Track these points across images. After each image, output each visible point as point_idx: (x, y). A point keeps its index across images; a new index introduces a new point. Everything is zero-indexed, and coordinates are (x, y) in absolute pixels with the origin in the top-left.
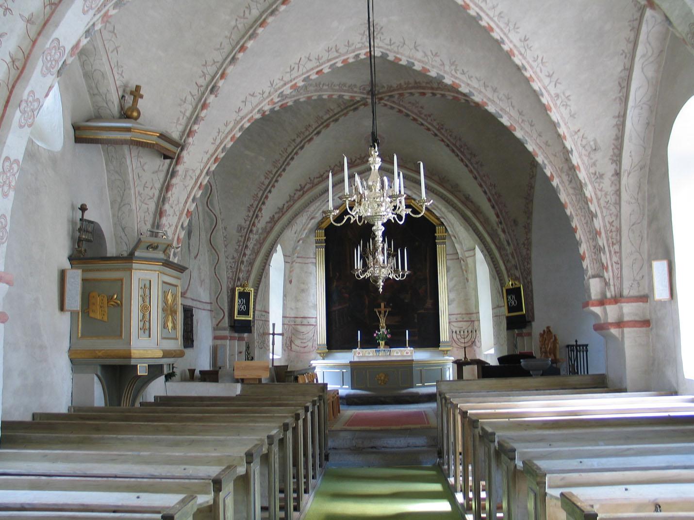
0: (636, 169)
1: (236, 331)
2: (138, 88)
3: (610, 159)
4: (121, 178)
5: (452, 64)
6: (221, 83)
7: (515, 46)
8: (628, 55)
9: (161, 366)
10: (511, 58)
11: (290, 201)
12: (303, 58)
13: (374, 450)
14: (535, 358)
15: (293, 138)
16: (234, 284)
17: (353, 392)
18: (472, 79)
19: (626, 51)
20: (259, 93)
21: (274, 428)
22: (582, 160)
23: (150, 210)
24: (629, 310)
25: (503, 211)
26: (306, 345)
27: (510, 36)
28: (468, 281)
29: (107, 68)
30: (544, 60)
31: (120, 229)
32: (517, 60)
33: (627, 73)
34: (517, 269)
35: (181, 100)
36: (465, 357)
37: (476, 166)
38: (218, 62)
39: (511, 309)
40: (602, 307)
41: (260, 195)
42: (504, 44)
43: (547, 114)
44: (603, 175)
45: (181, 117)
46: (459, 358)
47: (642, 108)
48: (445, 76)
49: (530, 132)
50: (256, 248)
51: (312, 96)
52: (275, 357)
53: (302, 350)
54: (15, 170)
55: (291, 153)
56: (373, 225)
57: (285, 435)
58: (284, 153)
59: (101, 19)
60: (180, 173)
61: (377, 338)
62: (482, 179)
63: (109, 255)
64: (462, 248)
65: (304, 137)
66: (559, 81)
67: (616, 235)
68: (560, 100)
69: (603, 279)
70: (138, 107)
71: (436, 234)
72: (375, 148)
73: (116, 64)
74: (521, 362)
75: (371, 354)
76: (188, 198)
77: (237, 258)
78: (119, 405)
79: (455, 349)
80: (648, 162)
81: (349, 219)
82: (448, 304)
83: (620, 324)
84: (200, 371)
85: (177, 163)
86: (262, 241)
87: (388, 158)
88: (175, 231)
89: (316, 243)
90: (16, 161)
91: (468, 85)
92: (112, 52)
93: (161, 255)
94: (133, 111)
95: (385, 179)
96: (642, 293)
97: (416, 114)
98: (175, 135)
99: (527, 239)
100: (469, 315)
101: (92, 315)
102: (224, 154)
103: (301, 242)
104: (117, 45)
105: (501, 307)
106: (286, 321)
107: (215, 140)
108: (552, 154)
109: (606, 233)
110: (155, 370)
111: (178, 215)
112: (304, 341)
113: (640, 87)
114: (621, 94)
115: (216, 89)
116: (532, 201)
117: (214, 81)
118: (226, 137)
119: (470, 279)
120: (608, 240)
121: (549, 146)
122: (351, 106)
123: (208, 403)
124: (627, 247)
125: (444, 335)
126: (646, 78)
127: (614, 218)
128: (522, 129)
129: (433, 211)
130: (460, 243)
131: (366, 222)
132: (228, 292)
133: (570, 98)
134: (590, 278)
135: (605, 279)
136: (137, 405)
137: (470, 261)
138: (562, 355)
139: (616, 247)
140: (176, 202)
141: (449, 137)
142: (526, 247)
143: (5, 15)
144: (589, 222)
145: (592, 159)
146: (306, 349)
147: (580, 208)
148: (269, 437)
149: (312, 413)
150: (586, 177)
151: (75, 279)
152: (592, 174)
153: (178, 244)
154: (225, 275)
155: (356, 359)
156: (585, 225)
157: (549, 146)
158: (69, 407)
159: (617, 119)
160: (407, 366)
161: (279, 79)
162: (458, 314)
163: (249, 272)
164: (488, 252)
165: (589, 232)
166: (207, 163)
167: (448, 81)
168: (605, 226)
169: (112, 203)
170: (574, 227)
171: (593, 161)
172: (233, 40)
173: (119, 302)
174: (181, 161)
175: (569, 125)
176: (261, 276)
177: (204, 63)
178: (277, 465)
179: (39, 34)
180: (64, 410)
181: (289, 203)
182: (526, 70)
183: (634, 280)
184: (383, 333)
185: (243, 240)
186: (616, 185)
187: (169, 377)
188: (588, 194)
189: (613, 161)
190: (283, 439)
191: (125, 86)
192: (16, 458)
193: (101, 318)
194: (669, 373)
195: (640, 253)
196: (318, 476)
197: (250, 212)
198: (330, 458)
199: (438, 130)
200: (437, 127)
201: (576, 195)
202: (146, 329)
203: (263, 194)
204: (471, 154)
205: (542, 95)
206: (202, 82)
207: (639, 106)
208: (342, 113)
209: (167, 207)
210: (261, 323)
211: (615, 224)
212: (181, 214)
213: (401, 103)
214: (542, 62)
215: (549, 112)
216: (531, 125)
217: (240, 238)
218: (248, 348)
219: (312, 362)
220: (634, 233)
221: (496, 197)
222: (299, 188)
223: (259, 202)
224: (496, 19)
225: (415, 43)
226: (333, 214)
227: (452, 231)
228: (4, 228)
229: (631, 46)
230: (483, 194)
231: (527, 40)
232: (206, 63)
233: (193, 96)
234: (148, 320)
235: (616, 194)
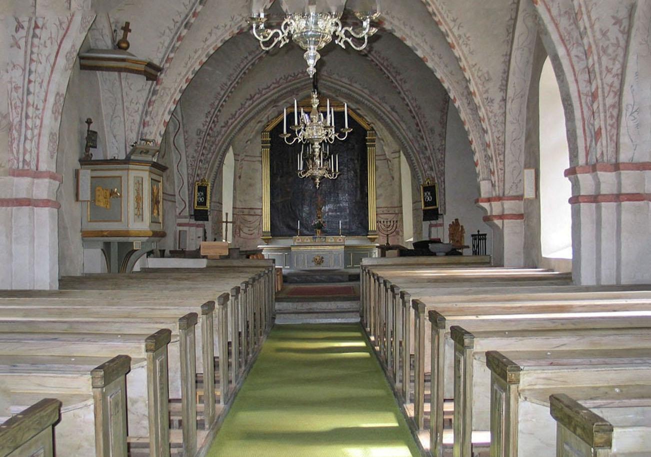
2: (128, 24)
4: (112, 96)
15: (245, 56)
25: (422, 122)
36: (388, 243)
39: (426, 204)
40: (489, 203)
41: (216, 104)
44: (493, 100)
46: (383, 244)
53: (249, 237)
62: (405, 94)
66: (461, 25)
68: (462, 40)
74: (428, 246)
75: (309, 241)
76: (165, 111)
79: (381, 238)
81: (297, 140)
83: (502, 217)
91: (391, 23)
98: (156, 62)
103: (249, 142)
109: (494, 146)
112: (251, 229)
113: (522, 34)
117: (188, 18)
120: (495, 151)
121: (453, 75)
124: (509, 157)
125: (372, 225)
126: (527, 27)
127: (501, 134)
128: (433, 60)
133: (470, 38)
134: (481, 180)
135: (492, 182)
138: (468, 241)
139: (501, 157)
141: (378, 58)
144: (482, 136)
147: (476, 125)
150: (480, 101)
168: (493, 140)
175: (469, 59)
185: (201, 142)
188: (481, 114)
189: (502, 90)
203: (219, 102)
205: (448, 36)
206: (180, 20)
211: (502, 139)
216: (440, 58)
217: (199, 140)
220: (515, 146)
221: (416, 109)
223: (216, 110)
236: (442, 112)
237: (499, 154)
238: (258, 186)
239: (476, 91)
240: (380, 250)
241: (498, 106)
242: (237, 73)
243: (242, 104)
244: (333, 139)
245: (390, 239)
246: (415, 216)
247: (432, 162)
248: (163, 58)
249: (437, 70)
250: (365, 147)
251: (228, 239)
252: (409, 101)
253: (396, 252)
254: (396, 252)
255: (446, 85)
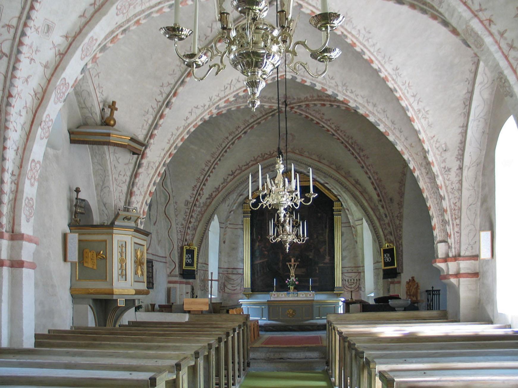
0: (474, 165)
1: (184, 278)
2: (114, 103)
3: (456, 157)
5: (344, 85)
6: (173, 100)
7: (389, 74)
8: (471, 82)
9: (134, 300)
10: (385, 82)
11: (224, 183)
12: (234, 80)
13: (282, 360)
14: (400, 299)
16: (183, 244)
17: (269, 322)
18: (358, 97)
19: (469, 79)
20: (202, 106)
21: (213, 340)
22: (436, 158)
23: (123, 191)
24: (464, 266)
25: (383, 192)
26: (235, 288)
27: (386, 66)
28: (356, 242)
29: (92, 88)
30: (410, 85)
31: (102, 204)
32: (391, 84)
33: (470, 95)
34: (391, 235)
35: (145, 112)
36: (352, 298)
37: (363, 158)
38: (171, 84)
39: (386, 264)
40: (445, 263)
41: (201, 178)
42: (381, 72)
43: (412, 124)
44: (450, 169)
45: (145, 125)
47: (479, 121)
48: (339, 94)
49: (399, 137)
50: (199, 217)
51: (241, 106)
52: (213, 297)
53: (233, 292)
54: (38, 168)
55: (225, 148)
56: (278, 210)
57: (219, 345)
58: (219, 147)
59: (91, 61)
60: (144, 165)
61: (288, 284)
63: (95, 223)
64: (353, 218)
65: (235, 135)
66: (421, 100)
67: (458, 213)
69: (447, 243)
70: (114, 117)
71: (334, 208)
72: (280, 158)
73: (98, 85)
74: (389, 302)
76: (150, 182)
77: (185, 224)
78: (105, 326)
79: (346, 293)
80: (483, 160)
81: (262, 205)
82: (342, 260)
83: (457, 275)
84: (159, 305)
85: (142, 158)
86: (203, 212)
87: (297, 151)
88: (141, 206)
89: (244, 214)
90: (39, 162)
91: (355, 101)
92: (95, 77)
93: (133, 224)
94: (110, 121)
95: (286, 180)
96: (474, 254)
97: (318, 119)
98: (141, 138)
99: (400, 213)
100: (357, 268)
101: (85, 265)
102: (176, 151)
103: (232, 212)
104: (98, 71)
105: (379, 262)
106: (221, 270)
107: (169, 140)
108: (415, 153)
109: (451, 211)
110: (130, 303)
111: (143, 195)
112: (234, 285)
113: (478, 106)
114: (465, 110)
115: (170, 104)
116: (404, 185)
117: (169, 98)
118: (177, 138)
119: (358, 241)
120: (452, 216)
121: (413, 147)
122: (270, 112)
123: (166, 326)
124: (465, 221)
125: (338, 283)
126: (483, 99)
127: (457, 200)
128: (394, 134)
129: (332, 190)
130: (352, 215)
131: (273, 207)
132: (178, 249)
133: (429, 112)
134: (438, 243)
135: (448, 244)
136: (117, 326)
137: (359, 228)
140: (141, 186)
142: (399, 218)
143: (30, 63)
145: (443, 157)
146: (235, 292)
147: (433, 193)
148: (209, 344)
149: (238, 334)
150: (438, 170)
151: (74, 239)
152: (443, 168)
153: (143, 215)
154: (175, 237)
155: (272, 299)
156: (436, 205)
157: (413, 147)
158: (71, 327)
159: (461, 129)
160: (310, 304)
161: (216, 96)
162: (349, 267)
163: (193, 235)
164: (371, 222)
165: (439, 210)
166: (164, 158)
167: (340, 98)
168: (450, 206)
169: (96, 187)
170: (428, 206)
171: (443, 159)
172: (182, 68)
173: (104, 256)
174: (145, 156)
175: (427, 132)
176: (203, 238)
177: (162, 85)
178: (214, 363)
179: (52, 75)
180: (68, 328)
181: (223, 184)
182: (396, 91)
183: (469, 244)
184: (293, 280)
186: (459, 176)
187: (138, 308)
188: (439, 183)
189: (458, 159)
190: (218, 347)
191: (104, 102)
192: (50, 353)
193: (92, 267)
194: (489, 309)
195: (474, 225)
196: (242, 376)
197: (194, 190)
198: (251, 365)
199: (335, 131)
200: (335, 128)
201: (431, 183)
202: (123, 274)
203: (204, 177)
204: (360, 149)
205: (408, 110)
206: (160, 98)
207: (477, 119)
208: (263, 118)
209: (135, 189)
210: (202, 272)
212: (146, 194)
213: (308, 111)
214: (409, 86)
215: (412, 123)
216: (401, 132)
217: (187, 210)
218: (193, 289)
219: (239, 301)
221: (377, 181)
222: (231, 173)
224: (375, 54)
225: (317, 69)
226: (251, 202)
227: (345, 205)
228: (32, 207)
229: (472, 75)
230: (368, 179)
231: (398, 69)
232: (163, 84)
233: (153, 109)
234: (124, 269)
235: (459, 183)
236: (400, 183)
237: (456, 219)
238: (240, 249)
239: (434, 161)
240: (345, 304)
241: (455, 174)
242: (220, 151)
243: (224, 179)
244: (299, 204)
245: (353, 294)
246: (376, 275)
247: (391, 227)
248: (147, 134)
249: (398, 143)
250: (333, 215)
251: (214, 294)
252: (371, 174)
253: (358, 305)
254: (358, 305)
255: (406, 157)
